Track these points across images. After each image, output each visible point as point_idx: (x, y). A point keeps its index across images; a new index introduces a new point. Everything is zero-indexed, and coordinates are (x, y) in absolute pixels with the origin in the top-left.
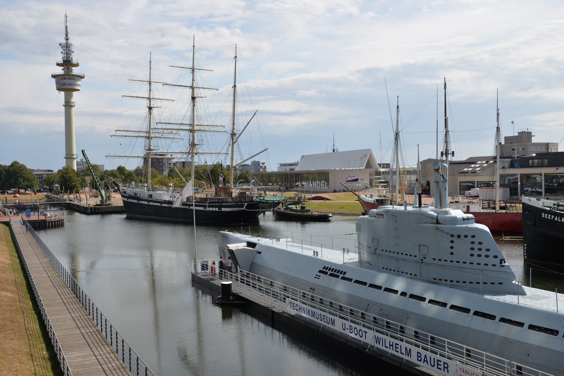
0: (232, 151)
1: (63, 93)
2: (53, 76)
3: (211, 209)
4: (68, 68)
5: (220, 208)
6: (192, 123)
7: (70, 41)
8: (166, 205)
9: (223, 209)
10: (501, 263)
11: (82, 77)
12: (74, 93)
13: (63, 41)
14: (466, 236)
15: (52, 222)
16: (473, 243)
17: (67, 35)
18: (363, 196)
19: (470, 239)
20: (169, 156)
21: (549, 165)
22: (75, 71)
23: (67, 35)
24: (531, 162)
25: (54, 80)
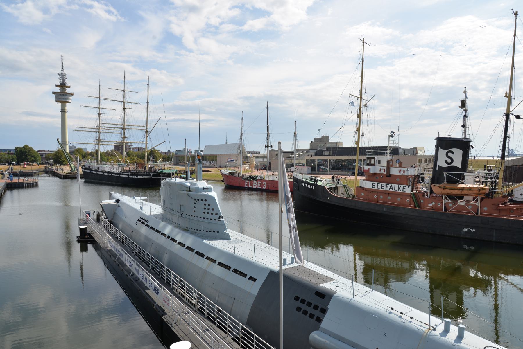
0: (146, 142)
1: (60, 104)
2: (53, 93)
3: (132, 177)
4: (63, 89)
5: (137, 176)
6: (123, 123)
7: (64, 72)
8: (106, 174)
9: (139, 177)
10: (219, 218)
11: (72, 95)
12: (67, 104)
13: (60, 72)
14: (202, 200)
15: (28, 184)
16: (205, 205)
17: (62, 68)
18: (222, 170)
19: (204, 202)
20: (130, 144)
21: (333, 155)
22: (68, 90)
23: (62, 68)
24: (323, 152)
25: (54, 95)
